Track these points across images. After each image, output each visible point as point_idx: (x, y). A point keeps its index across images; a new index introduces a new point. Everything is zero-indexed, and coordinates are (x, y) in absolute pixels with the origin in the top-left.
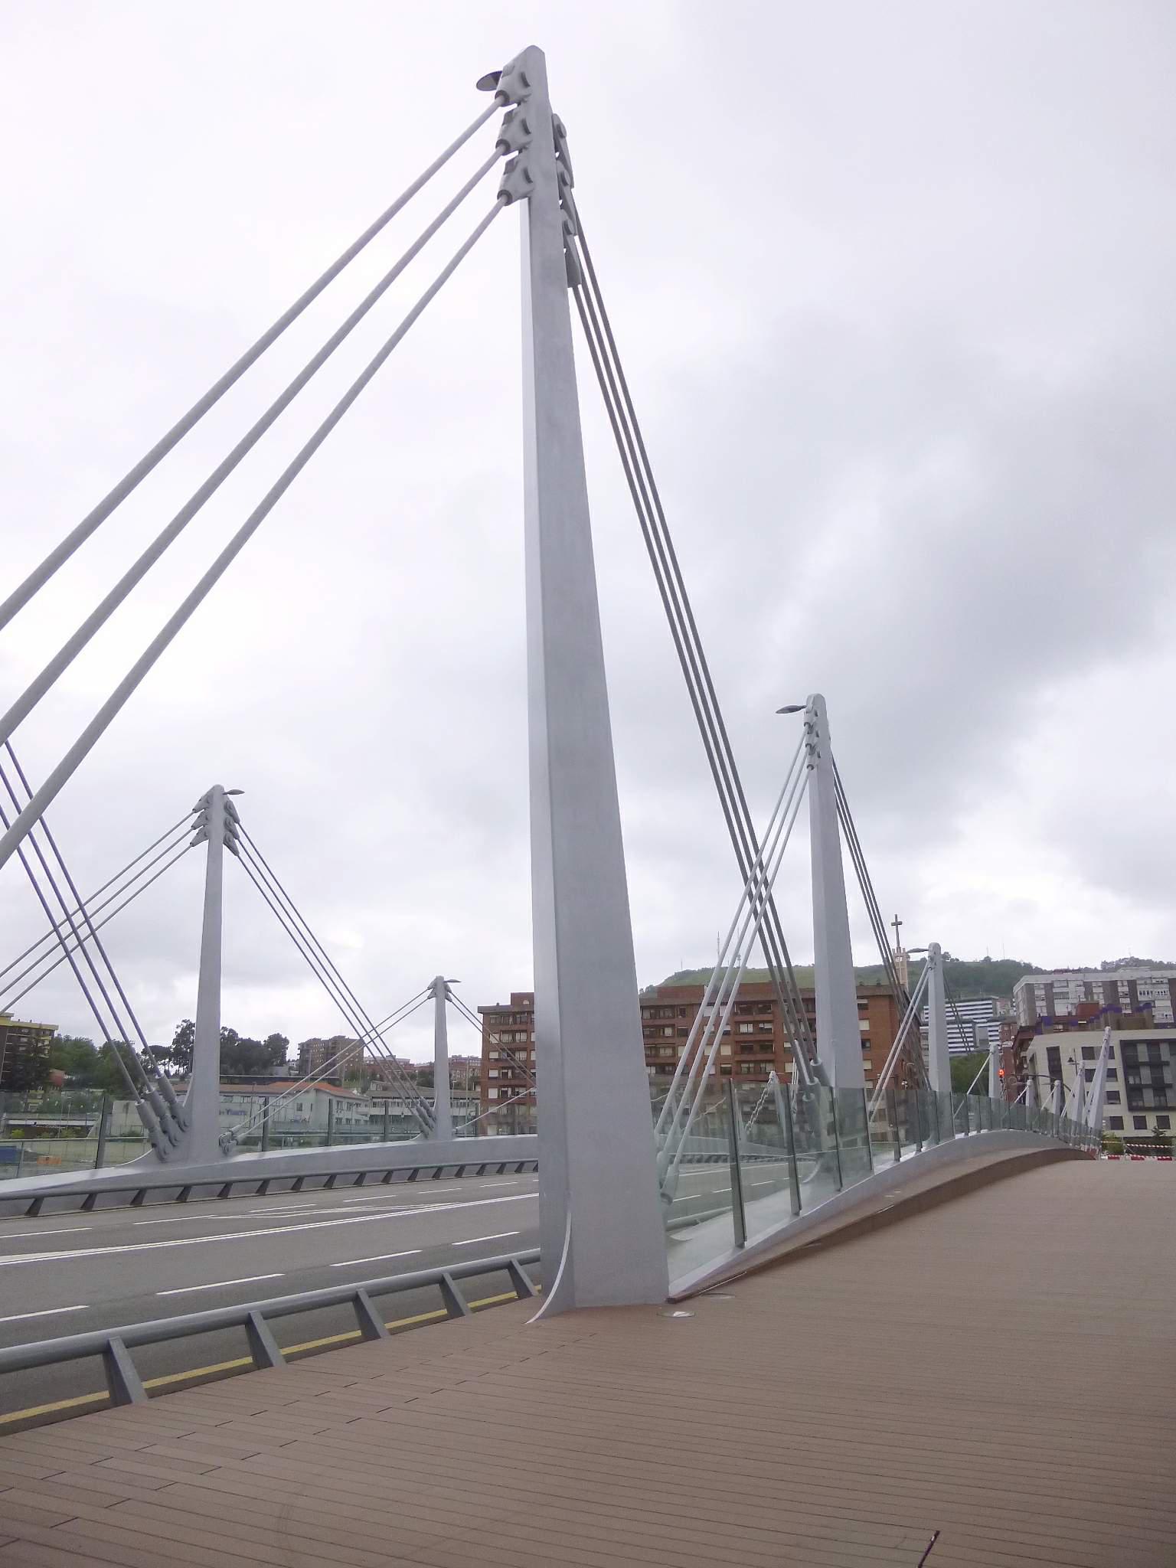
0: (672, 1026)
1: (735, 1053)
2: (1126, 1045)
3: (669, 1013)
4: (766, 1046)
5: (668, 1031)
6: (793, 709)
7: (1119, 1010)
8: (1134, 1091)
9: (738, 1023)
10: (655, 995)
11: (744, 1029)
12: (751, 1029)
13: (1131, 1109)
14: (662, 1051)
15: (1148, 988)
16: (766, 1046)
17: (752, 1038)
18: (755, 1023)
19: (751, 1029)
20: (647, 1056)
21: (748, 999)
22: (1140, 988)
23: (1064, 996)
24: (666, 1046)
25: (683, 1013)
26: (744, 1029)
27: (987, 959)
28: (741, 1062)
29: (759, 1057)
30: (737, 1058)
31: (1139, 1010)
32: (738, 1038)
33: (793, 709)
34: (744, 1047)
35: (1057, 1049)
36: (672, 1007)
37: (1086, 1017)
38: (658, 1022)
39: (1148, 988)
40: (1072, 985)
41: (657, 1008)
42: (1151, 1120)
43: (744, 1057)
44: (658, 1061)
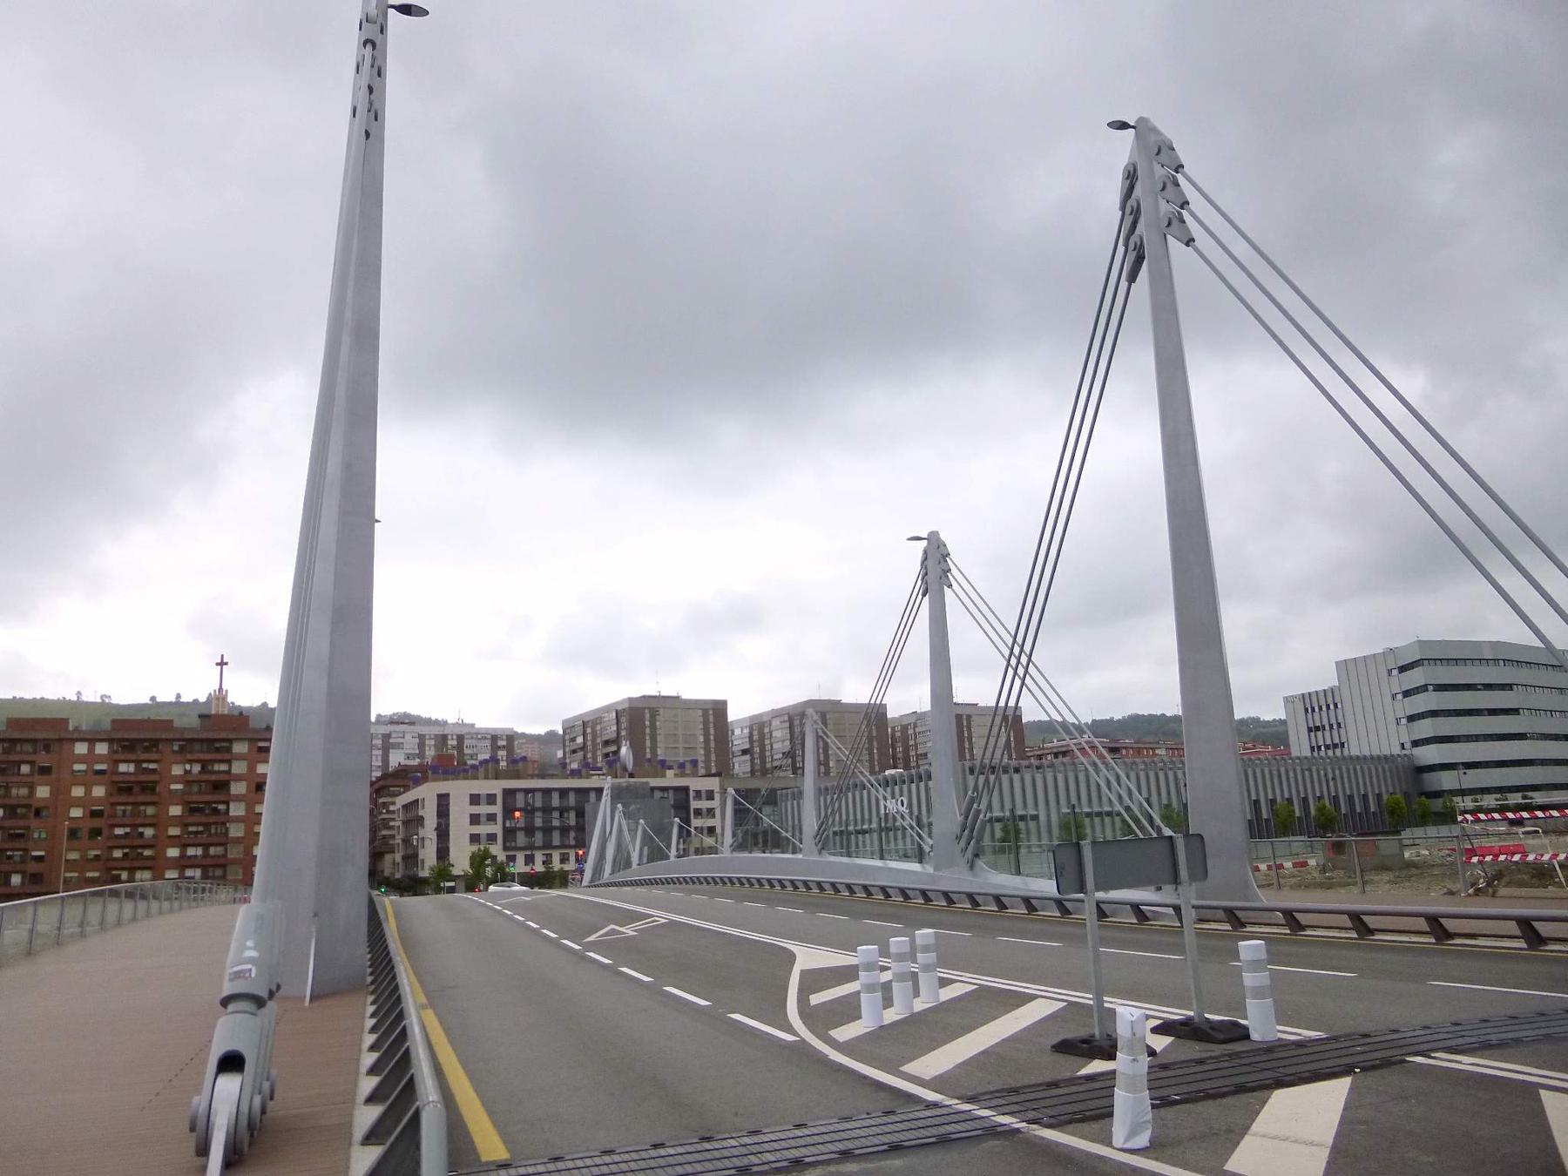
0: (32, 763)
1: (109, 794)
2: (509, 793)
3: (28, 748)
4: (149, 788)
5: (25, 769)
6: (1123, 126)
7: (497, 761)
8: (509, 833)
9: (117, 762)
10: (194, 722)
11: (123, 768)
12: (131, 768)
13: (505, 848)
14: (14, 791)
15: (474, 742)
16: (149, 788)
17: (132, 778)
18: (138, 762)
19: (131, 768)
20: (486, 778)
21: (17, 735)
22: (467, 742)
23: (398, 746)
24: (19, 785)
25: (47, 748)
26: (123, 768)
27: (265, 704)
28: (113, 804)
29: (141, 798)
30: (113, 800)
31: (515, 762)
32: (116, 778)
33: (1123, 126)
34: (122, 788)
35: (472, 796)
36: (34, 741)
37: (489, 768)
38: (12, 757)
39: (474, 742)
40: (408, 737)
41: (13, 741)
42: (539, 857)
43: (123, 799)
44: (7, 801)
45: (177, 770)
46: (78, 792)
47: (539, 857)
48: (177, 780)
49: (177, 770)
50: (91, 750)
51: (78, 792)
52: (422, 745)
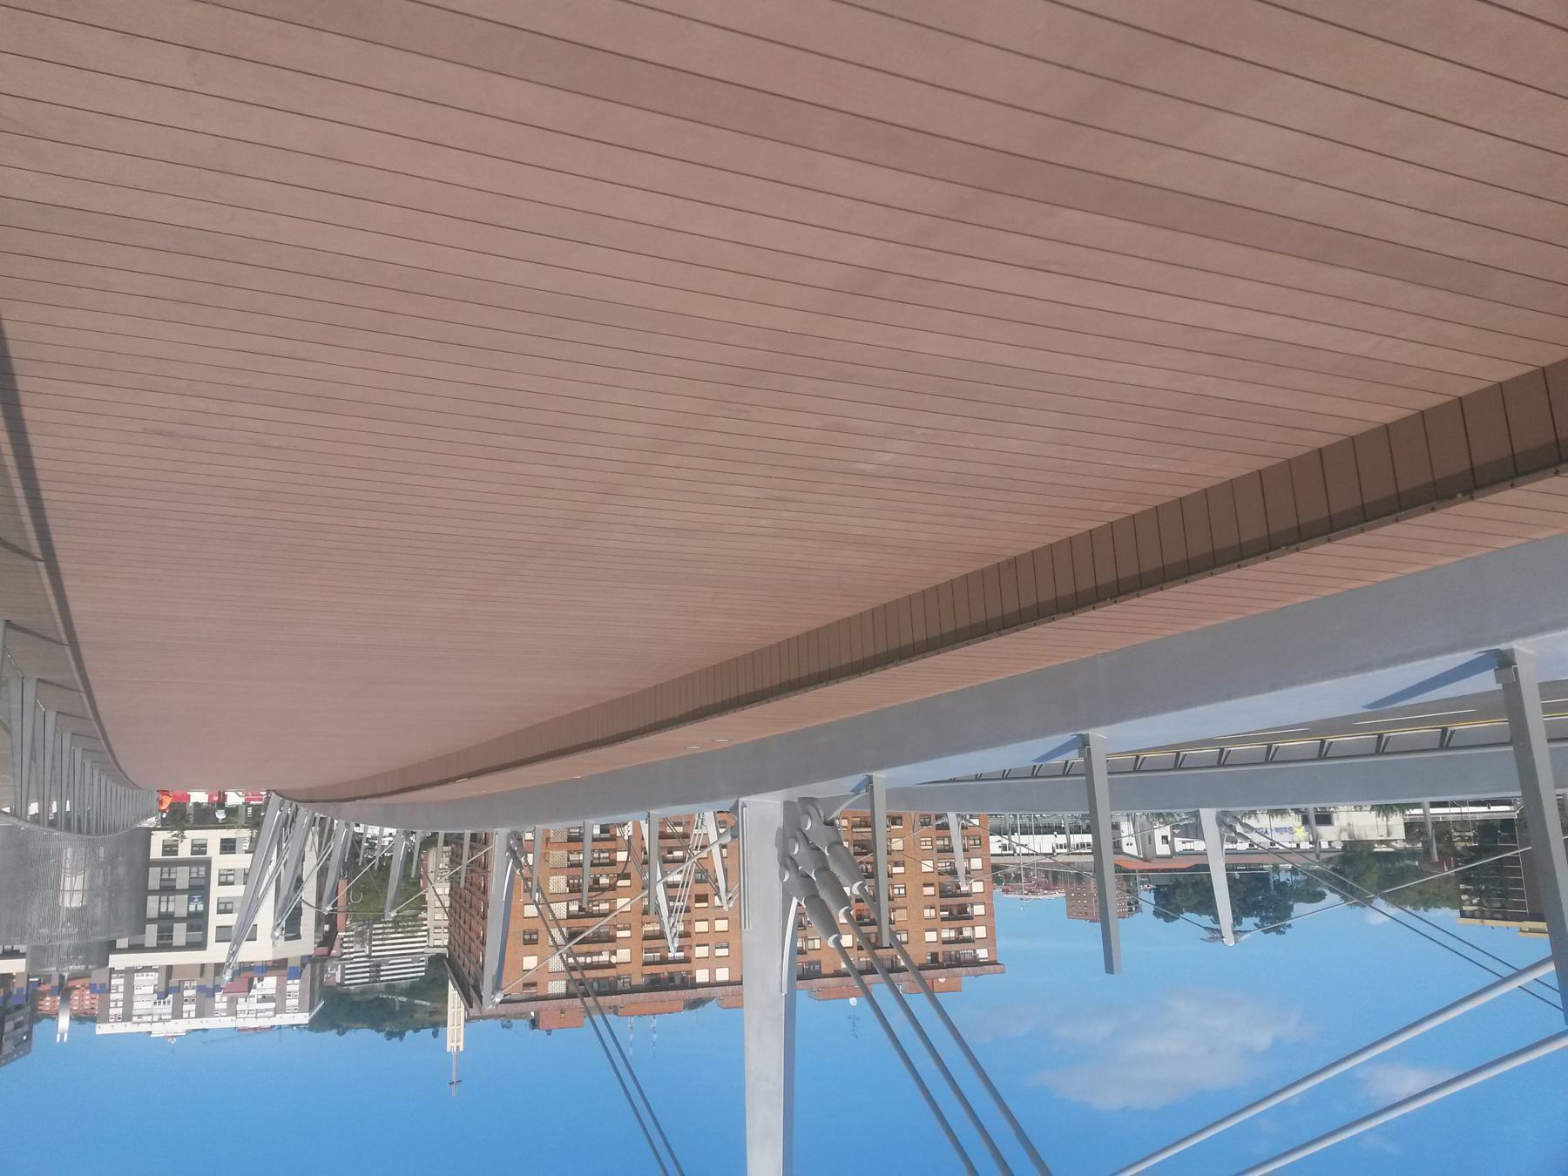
8: (199, 889)
13: (208, 863)
22: (168, 1009)
45: (623, 955)
46: (721, 925)
47: (184, 851)
48: (625, 942)
49: (623, 955)
50: (712, 974)
51: (721, 925)
52: (232, 1002)
